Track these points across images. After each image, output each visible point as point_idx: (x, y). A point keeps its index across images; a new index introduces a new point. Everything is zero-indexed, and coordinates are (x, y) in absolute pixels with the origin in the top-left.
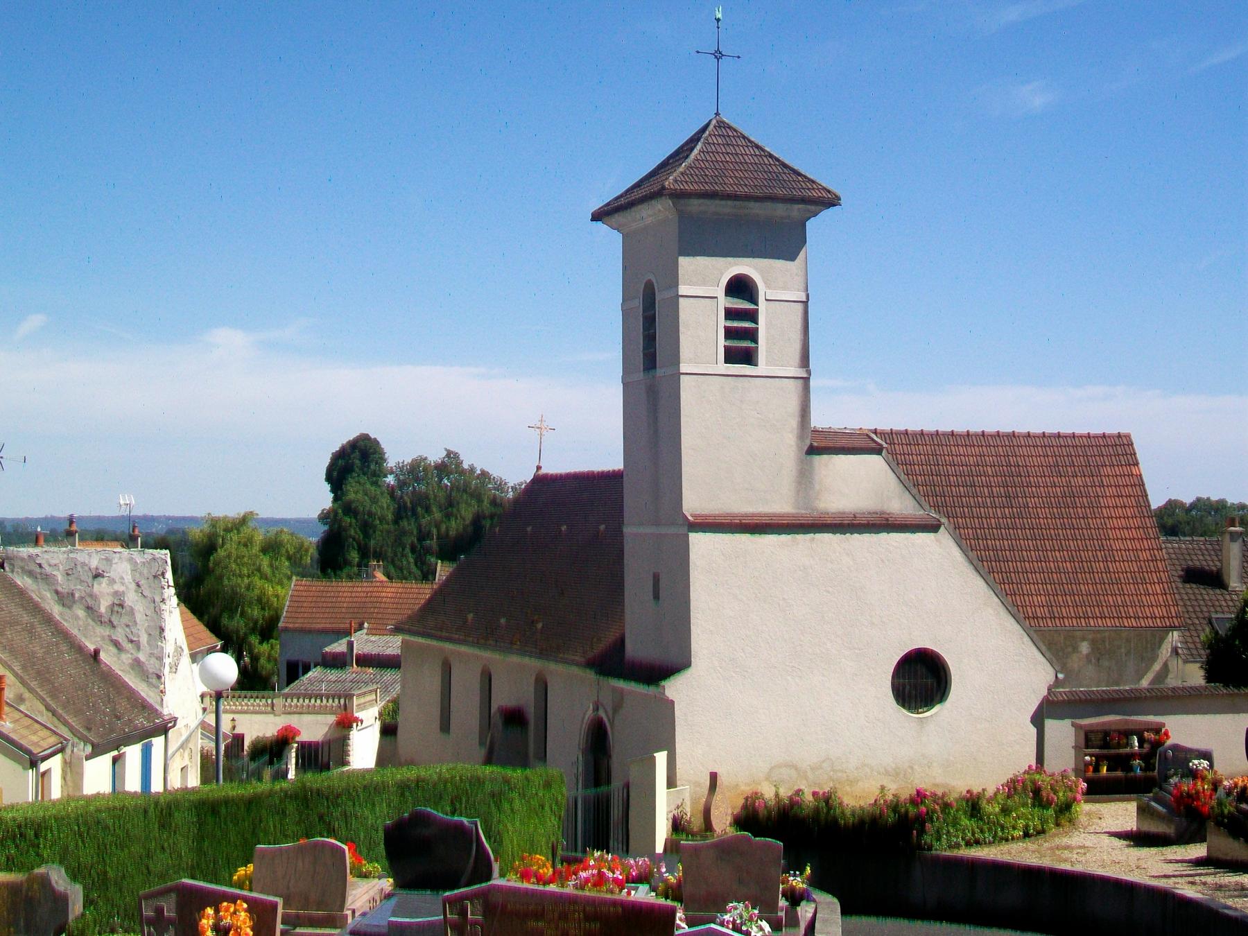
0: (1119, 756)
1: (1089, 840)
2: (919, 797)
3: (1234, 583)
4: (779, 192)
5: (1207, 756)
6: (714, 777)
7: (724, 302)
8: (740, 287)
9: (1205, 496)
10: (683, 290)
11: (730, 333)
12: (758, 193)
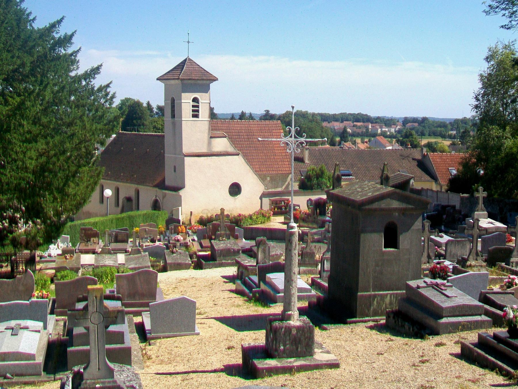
0: (279, 206)
1: (275, 224)
2: (240, 215)
3: (307, 161)
4: (204, 78)
5: (299, 206)
6: (191, 212)
7: (192, 103)
8: (195, 100)
9: (300, 110)
10: (183, 101)
11: (193, 111)
12: (200, 78)
